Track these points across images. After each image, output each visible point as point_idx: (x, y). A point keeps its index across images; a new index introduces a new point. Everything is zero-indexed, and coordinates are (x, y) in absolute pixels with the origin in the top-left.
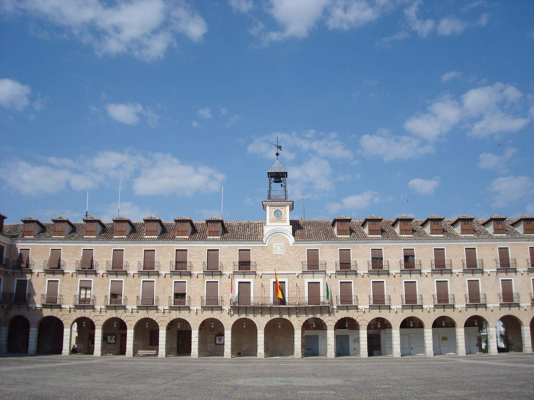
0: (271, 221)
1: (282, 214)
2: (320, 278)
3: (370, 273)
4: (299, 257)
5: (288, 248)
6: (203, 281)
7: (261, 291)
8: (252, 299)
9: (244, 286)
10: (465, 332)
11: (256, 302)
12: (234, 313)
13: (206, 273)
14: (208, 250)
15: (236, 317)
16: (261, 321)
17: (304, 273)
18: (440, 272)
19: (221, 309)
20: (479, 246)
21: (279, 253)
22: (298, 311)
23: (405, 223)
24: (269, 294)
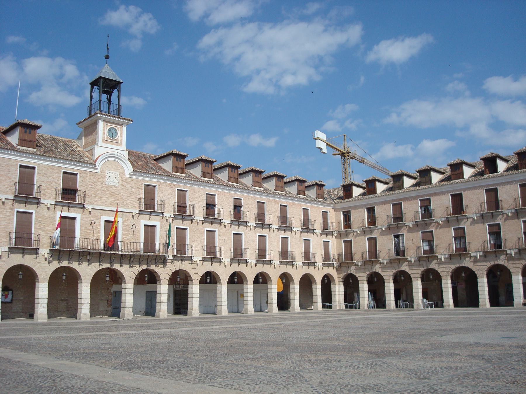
0: (105, 141)
2: (156, 221)
3: (204, 221)
4: (135, 193)
5: (123, 179)
6: (12, 209)
7: (88, 232)
8: (77, 241)
9: (67, 223)
10: (134, 289)
11: (83, 245)
12: (53, 260)
13: (17, 199)
14: (21, 166)
15: (56, 265)
16: (87, 271)
17: (140, 213)
18: (25, 200)
19: (35, 252)
20: (290, 204)
21: (112, 184)
22: (132, 259)
23: (28, 130)
24: (99, 236)
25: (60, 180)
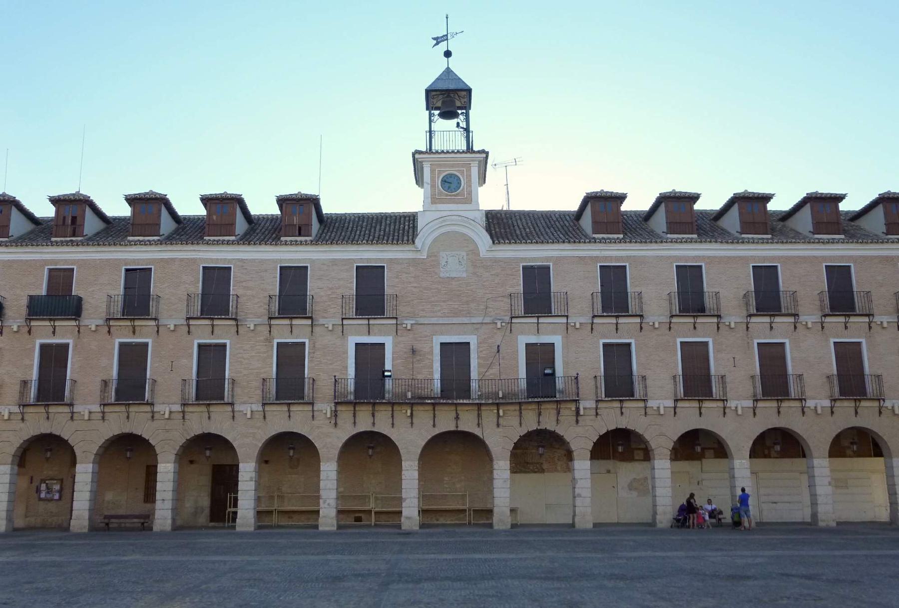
1: (460, 183)
11: (398, 390)
21: (454, 275)
24: (432, 373)
25: (352, 282)
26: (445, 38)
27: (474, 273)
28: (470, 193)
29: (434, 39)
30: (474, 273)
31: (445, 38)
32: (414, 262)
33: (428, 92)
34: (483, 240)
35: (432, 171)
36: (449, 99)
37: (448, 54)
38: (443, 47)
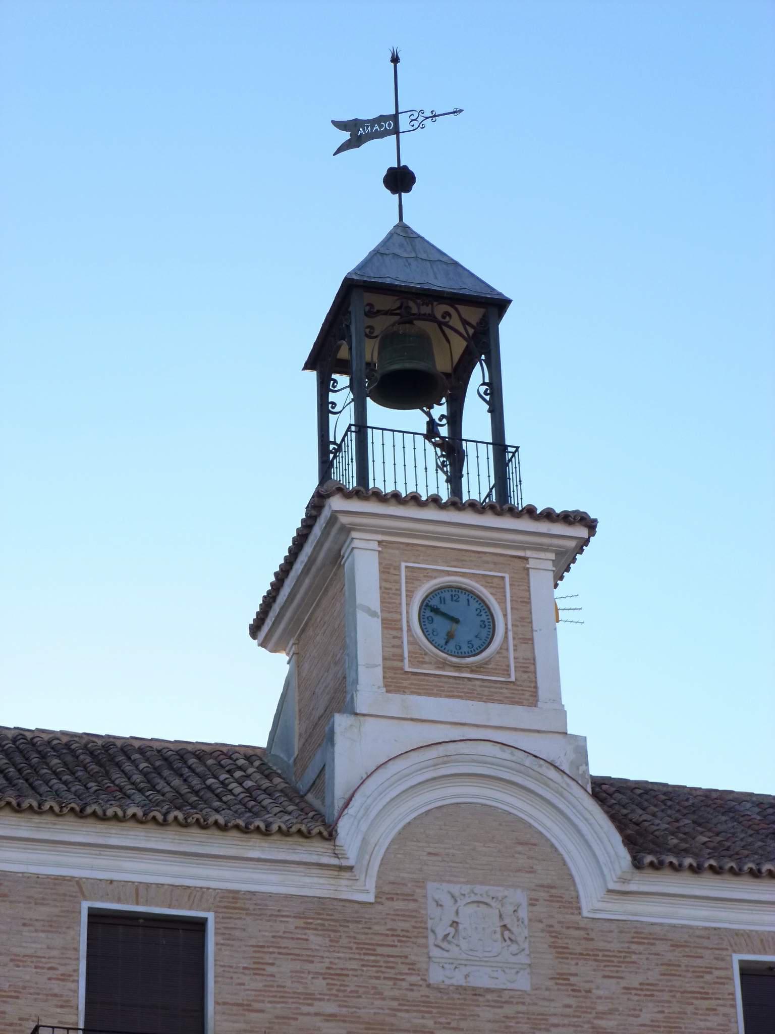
21: (482, 979)
26: (388, 126)
27: (562, 978)
28: (528, 666)
29: (341, 125)
30: (562, 978)
31: (388, 126)
32: (324, 914)
33: (351, 288)
34: (595, 854)
35: (387, 570)
36: (409, 334)
37: (399, 180)
38: (379, 155)
